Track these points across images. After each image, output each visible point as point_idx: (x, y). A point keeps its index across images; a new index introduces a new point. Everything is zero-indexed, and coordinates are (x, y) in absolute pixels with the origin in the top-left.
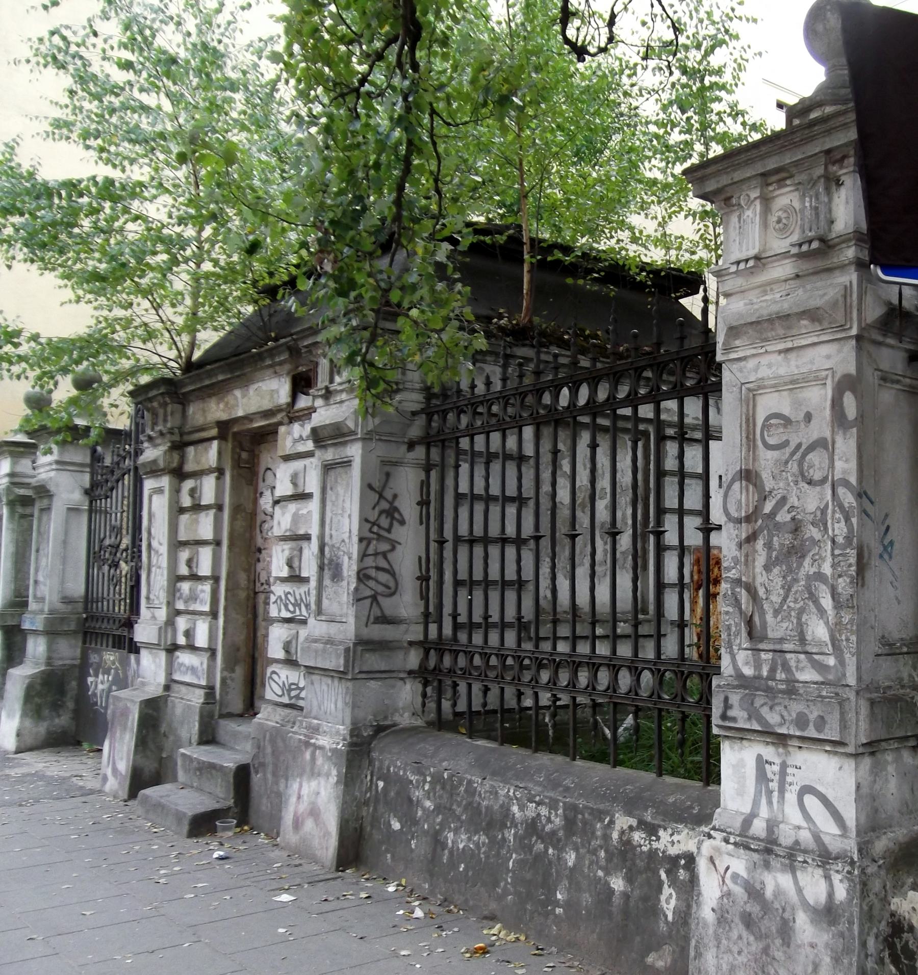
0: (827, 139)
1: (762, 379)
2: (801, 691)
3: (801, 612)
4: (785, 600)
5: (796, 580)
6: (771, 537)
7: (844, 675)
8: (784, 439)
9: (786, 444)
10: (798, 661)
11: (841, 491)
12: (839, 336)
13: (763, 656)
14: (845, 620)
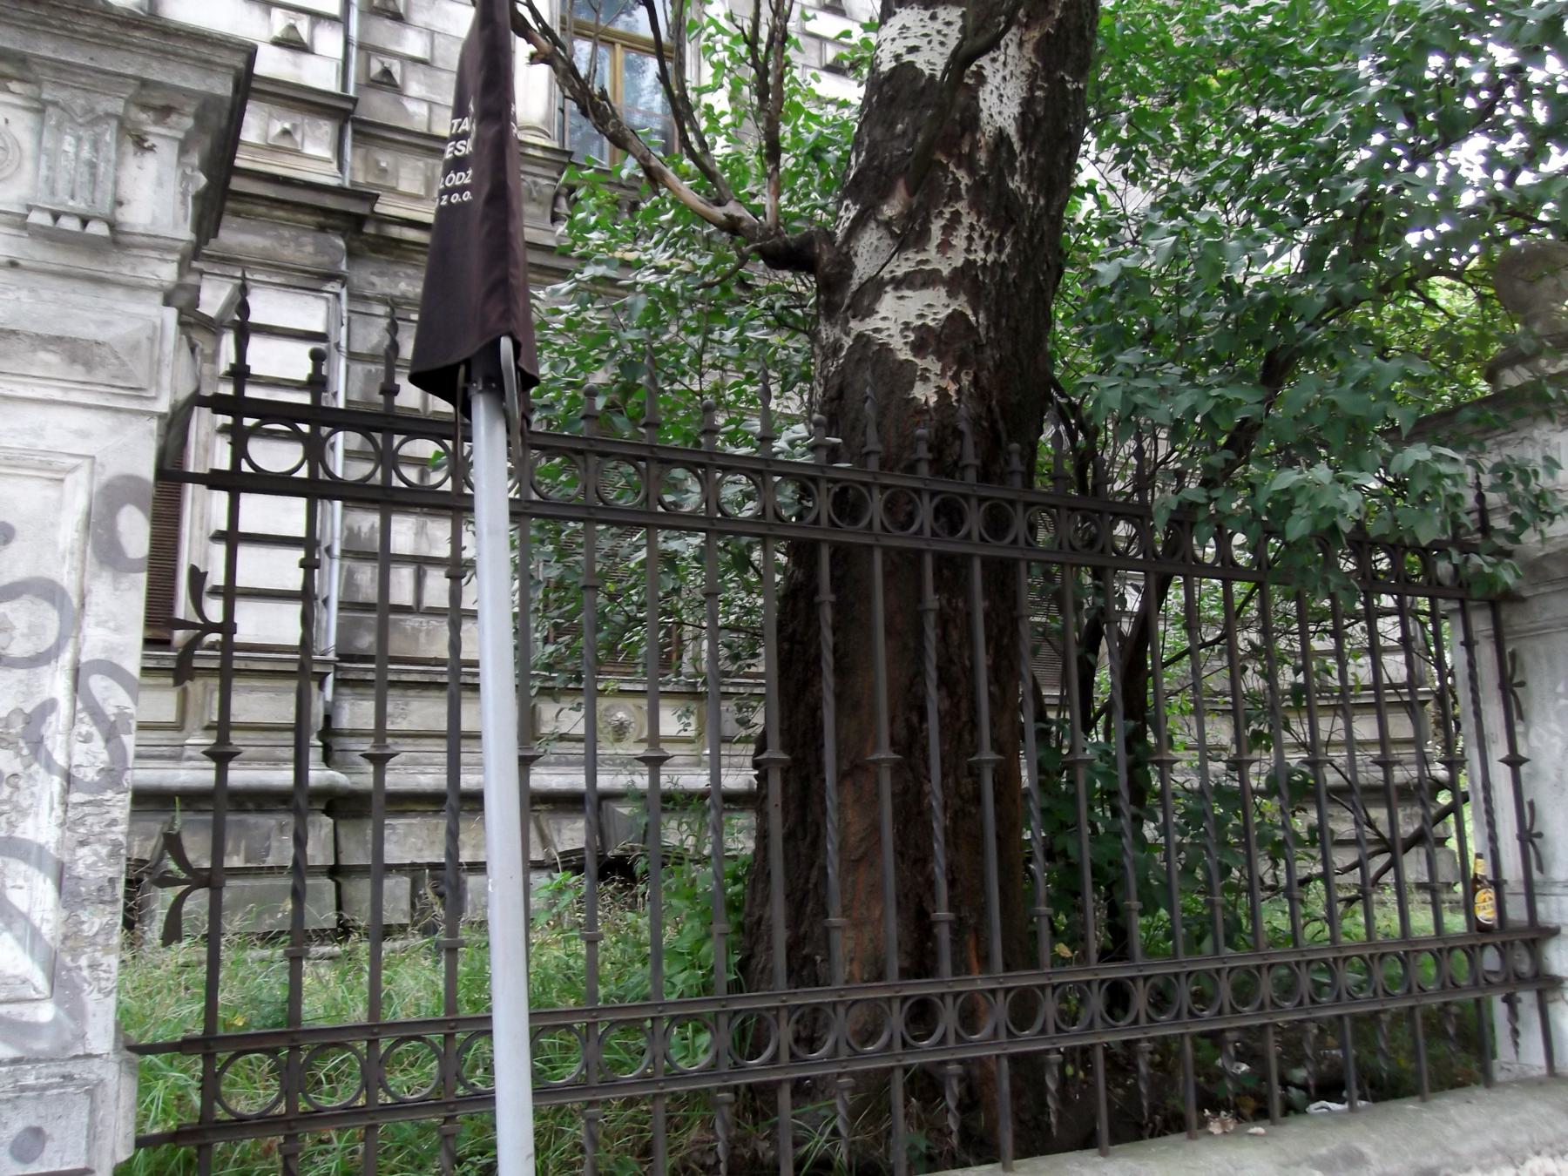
0: (155, 64)
7: (82, 1037)
11: (98, 684)
12: (122, 404)
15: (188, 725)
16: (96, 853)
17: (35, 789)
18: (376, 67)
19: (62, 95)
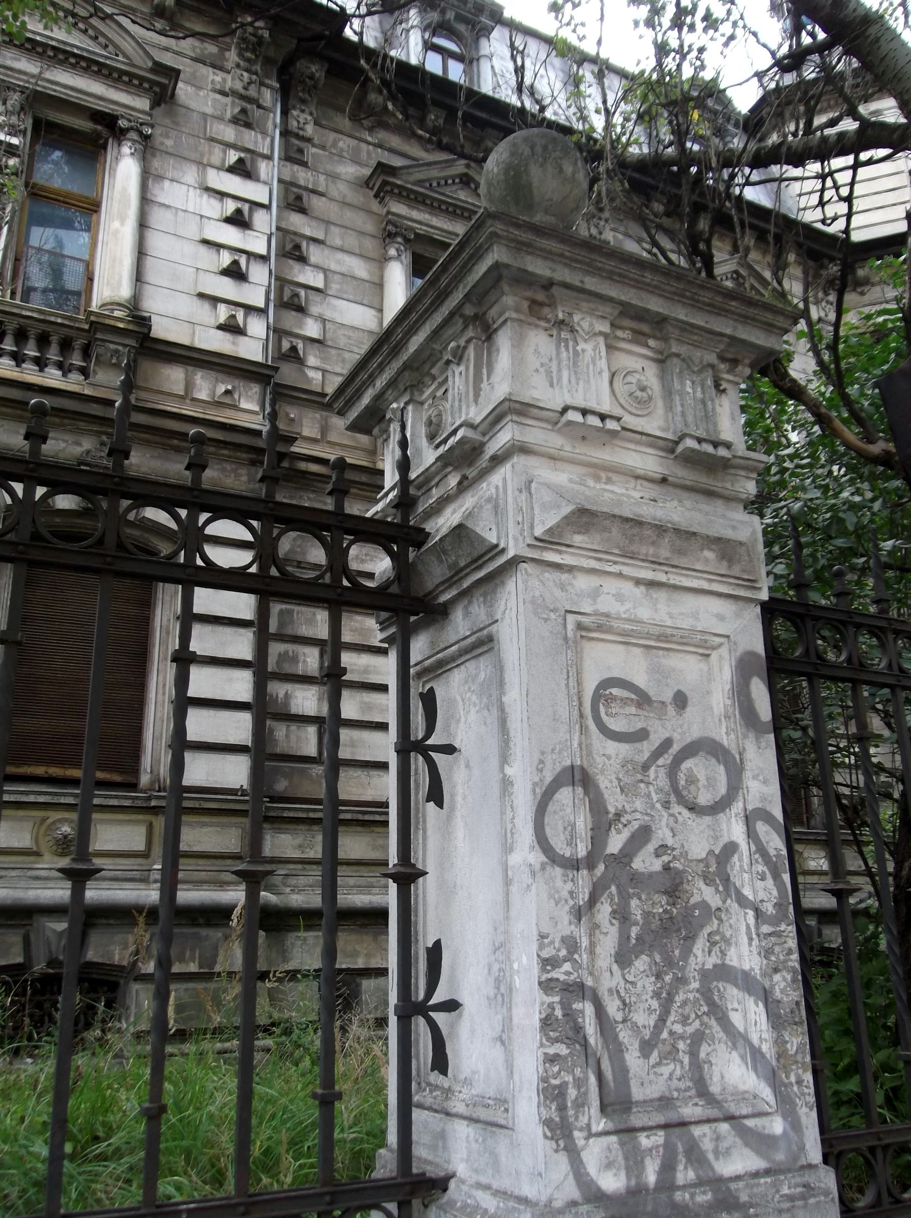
1: (607, 615)
2: (744, 1198)
3: (698, 1039)
4: (662, 1020)
5: (681, 981)
6: (625, 899)
7: (802, 1148)
8: (639, 726)
9: (641, 735)
10: (718, 1138)
11: (762, 828)
12: (742, 593)
13: (645, 1141)
14: (792, 1048)
15: (153, 854)
16: (785, 979)
17: (732, 921)
18: (286, 345)
19: (683, 350)
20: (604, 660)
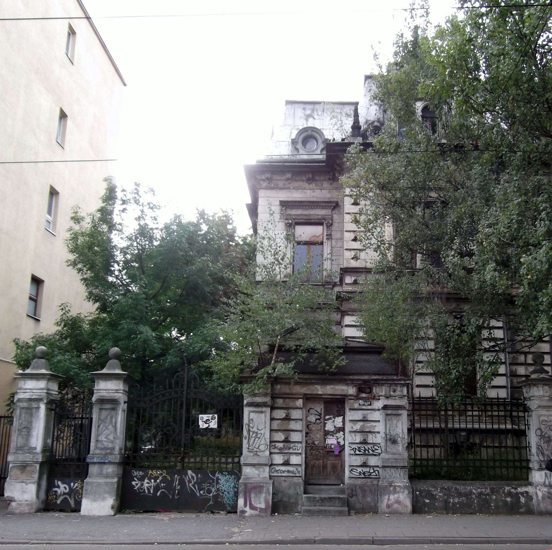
20: (542, 418)
